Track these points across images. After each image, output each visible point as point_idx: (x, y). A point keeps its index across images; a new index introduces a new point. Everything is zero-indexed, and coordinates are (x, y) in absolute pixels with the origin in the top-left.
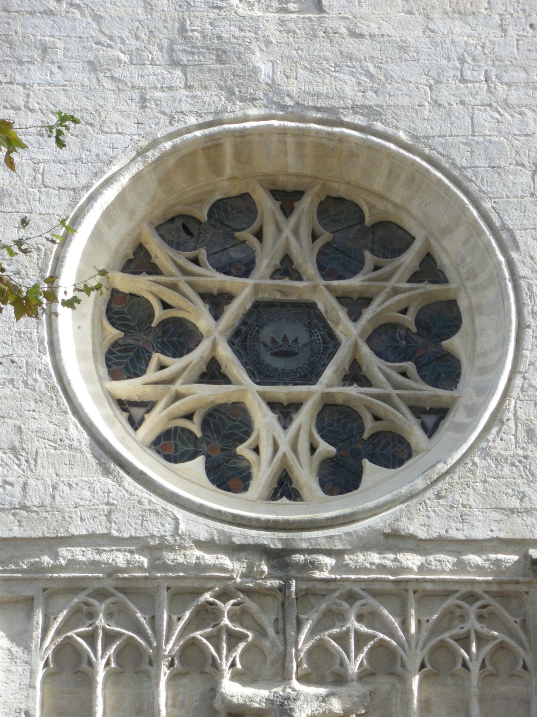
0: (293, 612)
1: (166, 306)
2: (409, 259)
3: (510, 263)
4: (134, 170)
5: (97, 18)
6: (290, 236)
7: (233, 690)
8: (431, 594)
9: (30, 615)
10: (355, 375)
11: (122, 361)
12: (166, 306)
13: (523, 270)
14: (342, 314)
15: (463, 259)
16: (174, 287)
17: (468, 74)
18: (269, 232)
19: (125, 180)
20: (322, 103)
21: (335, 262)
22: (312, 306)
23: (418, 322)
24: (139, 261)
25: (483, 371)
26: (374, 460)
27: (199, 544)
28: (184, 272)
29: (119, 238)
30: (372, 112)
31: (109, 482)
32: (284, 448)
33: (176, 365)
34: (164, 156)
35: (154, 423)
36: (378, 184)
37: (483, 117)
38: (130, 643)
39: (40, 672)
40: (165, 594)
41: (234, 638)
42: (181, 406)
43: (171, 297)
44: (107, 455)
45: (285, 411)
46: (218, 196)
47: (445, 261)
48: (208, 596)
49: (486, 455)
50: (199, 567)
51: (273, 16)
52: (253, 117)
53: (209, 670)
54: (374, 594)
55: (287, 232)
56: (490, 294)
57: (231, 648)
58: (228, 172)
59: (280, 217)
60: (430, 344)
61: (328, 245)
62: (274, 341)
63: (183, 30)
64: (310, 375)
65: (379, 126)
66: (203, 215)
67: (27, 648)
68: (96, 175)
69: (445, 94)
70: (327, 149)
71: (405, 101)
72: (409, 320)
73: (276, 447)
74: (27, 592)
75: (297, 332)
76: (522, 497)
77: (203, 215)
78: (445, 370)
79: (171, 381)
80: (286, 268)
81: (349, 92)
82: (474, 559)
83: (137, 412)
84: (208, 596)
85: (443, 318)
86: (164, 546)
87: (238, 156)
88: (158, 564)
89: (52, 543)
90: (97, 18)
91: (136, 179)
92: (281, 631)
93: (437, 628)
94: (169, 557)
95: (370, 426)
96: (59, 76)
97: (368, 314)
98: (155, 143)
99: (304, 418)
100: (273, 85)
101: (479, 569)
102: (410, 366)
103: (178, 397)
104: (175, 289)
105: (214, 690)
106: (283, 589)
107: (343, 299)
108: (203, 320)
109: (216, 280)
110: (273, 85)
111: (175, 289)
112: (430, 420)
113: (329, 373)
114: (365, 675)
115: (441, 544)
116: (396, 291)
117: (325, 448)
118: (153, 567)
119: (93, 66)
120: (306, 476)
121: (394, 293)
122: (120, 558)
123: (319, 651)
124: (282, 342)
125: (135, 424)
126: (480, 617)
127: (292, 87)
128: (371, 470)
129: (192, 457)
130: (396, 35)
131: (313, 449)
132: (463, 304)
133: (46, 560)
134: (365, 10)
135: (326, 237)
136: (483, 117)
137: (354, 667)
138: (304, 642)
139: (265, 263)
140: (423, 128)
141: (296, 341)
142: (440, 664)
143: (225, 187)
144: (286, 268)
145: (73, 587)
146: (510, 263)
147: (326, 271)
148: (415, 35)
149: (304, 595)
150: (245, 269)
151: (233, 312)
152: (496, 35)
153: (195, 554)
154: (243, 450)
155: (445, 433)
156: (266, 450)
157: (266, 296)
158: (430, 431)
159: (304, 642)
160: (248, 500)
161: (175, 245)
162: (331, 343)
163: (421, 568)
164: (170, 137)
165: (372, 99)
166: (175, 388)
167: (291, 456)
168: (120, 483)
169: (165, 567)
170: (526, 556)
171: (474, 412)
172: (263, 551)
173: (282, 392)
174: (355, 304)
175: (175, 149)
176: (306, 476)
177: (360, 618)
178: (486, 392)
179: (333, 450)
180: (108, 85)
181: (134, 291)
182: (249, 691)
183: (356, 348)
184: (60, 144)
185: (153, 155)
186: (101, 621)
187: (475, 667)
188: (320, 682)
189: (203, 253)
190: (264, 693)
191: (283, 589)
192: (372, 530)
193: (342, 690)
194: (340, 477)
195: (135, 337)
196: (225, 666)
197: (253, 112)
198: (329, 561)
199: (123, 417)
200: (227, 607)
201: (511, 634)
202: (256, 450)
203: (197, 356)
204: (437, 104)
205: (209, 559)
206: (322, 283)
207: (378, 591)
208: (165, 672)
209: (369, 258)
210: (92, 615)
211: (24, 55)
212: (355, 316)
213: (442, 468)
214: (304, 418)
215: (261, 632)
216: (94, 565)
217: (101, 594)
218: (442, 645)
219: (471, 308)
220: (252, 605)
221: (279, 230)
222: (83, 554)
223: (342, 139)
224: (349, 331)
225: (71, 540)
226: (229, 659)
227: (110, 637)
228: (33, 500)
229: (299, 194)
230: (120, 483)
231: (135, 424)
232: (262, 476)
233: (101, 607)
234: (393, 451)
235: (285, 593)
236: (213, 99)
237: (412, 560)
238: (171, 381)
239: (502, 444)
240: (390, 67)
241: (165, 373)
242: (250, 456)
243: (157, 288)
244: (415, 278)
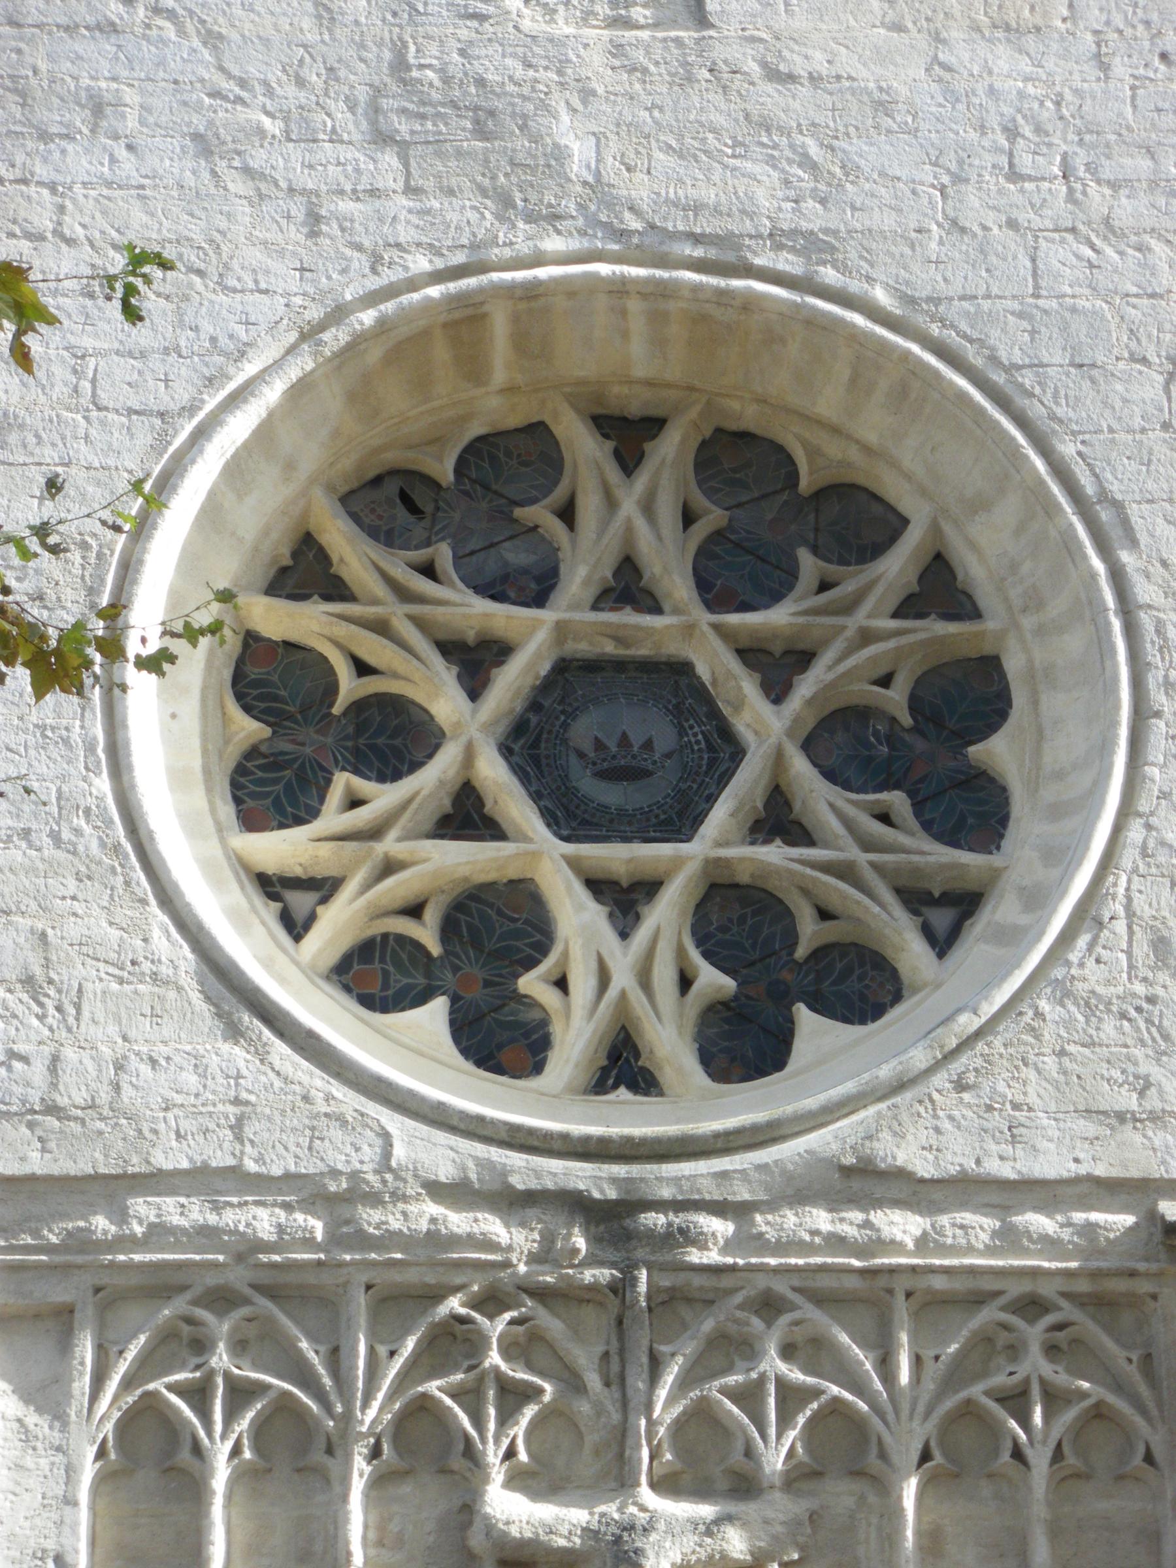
0: (641, 1338)
1: (363, 669)
2: (897, 567)
3: (1117, 576)
4: (294, 372)
5: (213, 39)
6: (635, 516)
7: (509, 1509)
8: (943, 1298)
9: (65, 1344)
10: (777, 819)
11: (267, 789)
12: (363, 669)
13: (1144, 591)
14: (749, 687)
15: (1014, 567)
16: (381, 628)
17: (1025, 162)
18: (589, 507)
19: (273, 393)
20: (705, 225)
21: (734, 573)
22: (684, 669)
23: (915, 703)
24: (303, 571)
25: (1057, 811)
26: (820, 1006)
27: (436, 1190)
28: (404, 594)
29: (260, 520)
30: (814, 245)
31: (238, 1054)
32: (623, 979)
33: (385, 797)
34: (358, 341)
35: (337, 924)
36: (828, 403)
37: (1059, 256)
38: (284, 1406)
39: (88, 1471)
40: (361, 1300)
41: (513, 1396)
42: (396, 888)
43: (373, 649)
44: (234, 995)
45: (624, 899)
46: (477, 429)
47: (975, 571)
48: (455, 1304)
49: (1064, 994)
50: (436, 1239)
52: (553, 255)
53: (457, 1465)
54: (820, 1299)
55: (629, 507)
56: (1074, 643)
57: (506, 1418)
58: (500, 376)
59: (613, 474)
60: (941, 752)
61: (717, 536)
63: (400, 65)
64: (679, 821)
65: (829, 275)
66: (445, 470)
67: (59, 1417)
68: (211, 382)
69: (974, 206)
70: (716, 326)
71: (888, 221)
72: (896, 699)
73: (604, 979)
74: (60, 1294)
75: (650, 727)
76: (1144, 1086)
77: (445, 470)
78: (974, 810)
79: (374, 833)
80: (627, 587)
81: (764, 202)
82: (1039, 1222)
83: (300, 901)
84: (455, 1304)
85: (970, 696)
86: (358, 1193)
87: (521, 342)
88: (345, 1234)
89: (113, 1188)
90: (213, 39)
91: (299, 391)
92: (616, 1380)
93: (958, 1374)
94: (371, 1218)
95: (810, 932)
96: (128, 165)
97: (806, 687)
98: (339, 314)
99: (665, 915)
100: (597, 185)
101: (1050, 1245)
102: (897, 800)
103: (389, 868)
104: (382, 632)
105: (468, 1509)
106: (620, 1288)
107: (751, 653)
108: (444, 699)
109: (474, 612)
110: (597, 185)
111: (382, 632)
112: (941, 919)
113: (721, 815)
114: (800, 1477)
115: (966, 1189)
116: (866, 637)
117: (713, 980)
118: (335, 1240)
119: (204, 145)
120: (670, 1042)
121: (863, 641)
122: (263, 1221)
123: (700, 1423)
124: (619, 748)
125: (296, 927)
126: (1052, 1350)
127: (640, 189)
128: (812, 1029)
129: (421, 998)
130: (867, 77)
131: (685, 982)
132: (1013, 665)
133: (101, 1224)
134: (800, 22)
135: (713, 517)
136: (1059, 256)
138: (665, 1404)
139: (580, 575)
140: (925, 280)
141: (648, 745)
142: (964, 1451)
143: (492, 409)
144: (627, 587)
145: (160, 1284)
146: (1117, 576)
147: (714, 592)
148: (908, 77)
149: (666, 1302)
150: (538, 588)
151: (510, 682)
152: (1086, 76)
153: (427, 1212)
154: (532, 983)
155: (974, 947)
156: (582, 983)
157: (582, 648)
158: (942, 943)
159: (665, 1404)
161: (384, 535)
162: (725, 749)
163: (923, 1243)
164: (372, 299)
165: (814, 217)
166: (382, 848)
167: (637, 998)
168: (262, 1056)
169: (362, 1241)
170: (1153, 1217)
171: (1039, 900)
172: (576, 1204)
173: (618, 856)
174: (778, 665)
175: (383, 326)
176: (670, 1042)
177: (788, 1352)
178: (1063, 858)
179: (728, 984)
180: (237, 185)
181: (294, 636)
182: (546, 1511)
183: (779, 760)
184: (132, 314)
185: (335, 338)
186: (221, 1359)
187: (1039, 1459)
188: (700, 1492)
189: (444, 554)
190: (579, 1516)
191: (620, 1288)
192: (814, 1160)
193: (750, 1509)
194: (745, 1044)
195: (297, 736)
196: (493, 1455)
197: (554, 244)
198: (720, 1227)
199: (269, 912)
200: (497, 1327)
201: (1119, 1386)
202: (562, 984)
203: (431, 779)
204: (956, 227)
205: (458, 1221)
206: (705, 618)
207: (828, 1293)
208: (360, 1469)
209: (808, 563)
210: (201, 1346)
211: (53, 119)
212: (777, 692)
213: (968, 1023)
214: (665, 915)
215: (572, 1382)
216: (206, 1235)
217: (222, 1300)
218: (969, 1411)
220: (551, 1324)
221: (611, 503)
222: (181, 1211)
223: (750, 303)
224: (765, 724)
225: (156, 1182)
226: (501, 1442)
227: (240, 1394)
228: (73, 1094)
229: (654, 425)
230: (262, 1056)
231: (296, 927)
232: (575, 1040)
233: (222, 1328)
234: (861, 987)
235: (624, 1297)
236: (467, 217)
237: (902, 1226)
238: (374, 833)
239: (1100, 970)
240: (854, 146)
241: (361, 816)
242: (548, 997)
243: (343, 630)
244: (910, 607)
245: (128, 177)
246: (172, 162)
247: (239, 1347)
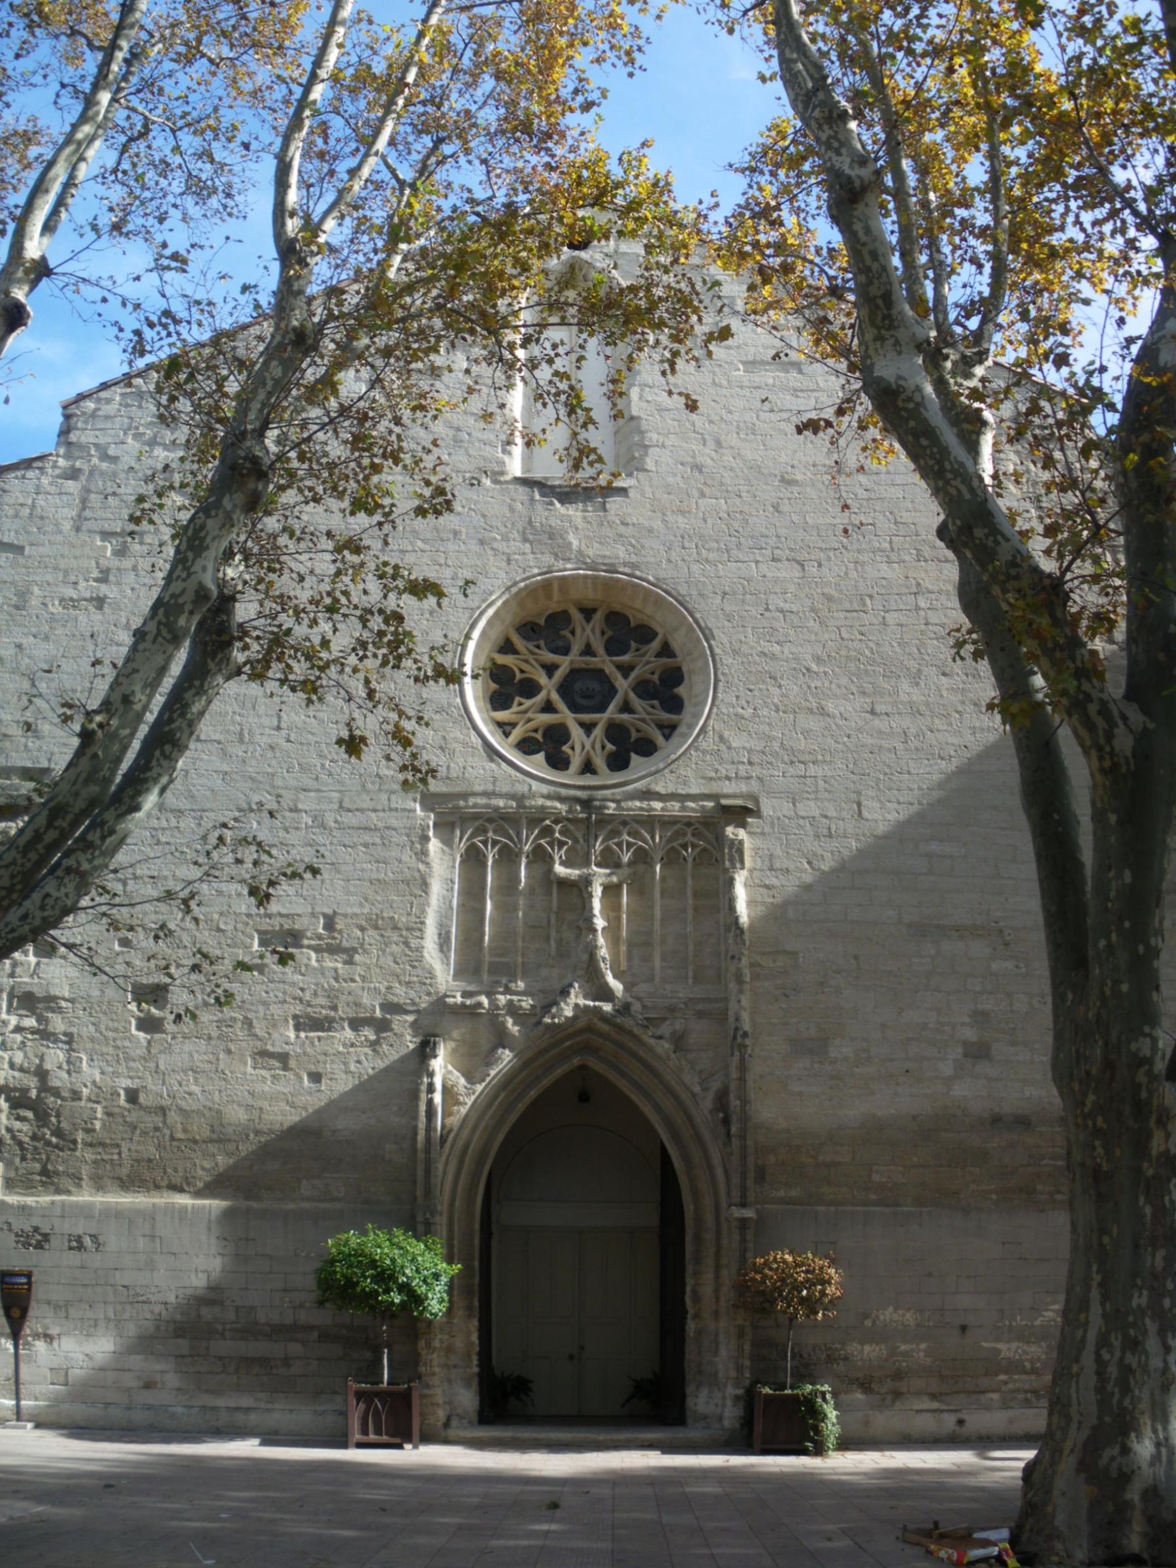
0: (593, 831)
1: (522, 671)
2: (655, 645)
3: (710, 647)
4: (504, 598)
5: (484, 516)
6: (589, 633)
7: (560, 870)
8: (666, 822)
9: (453, 831)
10: (626, 708)
11: (498, 701)
12: (522, 671)
13: (717, 651)
14: (619, 676)
16: (526, 661)
17: (686, 544)
18: (578, 630)
19: (499, 603)
20: (607, 561)
21: (615, 647)
22: (602, 671)
23: (660, 679)
24: (507, 647)
25: (696, 705)
26: (637, 753)
27: (543, 797)
28: (532, 653)
29: (496, 634)
30: (634, 566)
31: (493, 765)
32: (588, 747)
33: (528, 703)
34: (520, 590)
35: (517, 734)
36: (638, 604)
37: (695, 568)
38: (506, 845)
39: (458, 860)
40: (524, 822)
41: (561, 844)
42: (531, 725)
43: (525, 666)
44: (492, 753)
45: (588, 728)
47: (675, 646)
48: (548, 822)
49: (697, 749)
50: (543, 807)
51: (579, 514)
52: (569, 569)
53: (549, 860)
54: (637, 822)
55: (588, 631)
56: (699, 664)
57: (560, 849)
60: (668, 691)
61: (610, 638)
63: (530, 522)
64: (602, 708)
65: (638, 573)
66: (542, 622)
67: (451, 847)
68: (484, 601)
69: (674, 556)
70: (610, 586)
71: (652, 560)
72: (655, 678)
73: (583, 747)
74: (451, 818)
75: (594, 686)
76: (717, 771)
77: (542, 622)
78: (675, 705)
79: (525, 712)
80: (588, 651)
81: (621, 555)
82: (691, 804)
83: (508, 728)
84: (548, 822)
85: (674, 677)
86: (523, 797)
87: (561, 589)
88: (521, 805)
89: (465, 796)
90: (484, 516)
91: (504, 603)
92: (587, 840)
93: (670, 840)
94: (527, 803)
95: (634, 735)
96: (463, 547)
97: (633, 675)
98: (515, 584)
99: (598, 732)
100: (580, 552)
101: (693, 810)
102: (656, 703)
103: (529, 720)
104: (525, 662)
105: (550, 869)
106: (588, 819)
107: (620, 667)
108: (543, 679)
109: (550, 657)
110: (580, 552)
111: (525, 662)
112: (667, 731)
113: (612, 707)
114: (631, 863)
115: (673, 796)
116: (648, 663)
117: (610, 747)
118: (518, 807)
119: (482, 542)
120: (599, 762)
121: (647, 663)
122: (501, 803)
123: (607, 851)
124: (584, 691)
125: (507, 735)
126: (694, 835)
127: (590, 552)
128: (635, 759)
129: (537, 752)
130: (646, 524)
131: (603, 747)
132: (685, 669)
133: (462, 803)
134: (630, 510)
135: (609, 633)
136: (695, 568)
137: (626, 858)
138: (598, 846)
139: (577, 647)
140: (662, 574)
142: (671, 858)
143: (554, 607)
144: (588, 651)
145: (476, 817)
146: (710, 647)
147: (610, 652)
148: (657, 524)
149: (598, 822)
150: (566, 651)
151: (559, 675)
152: (700, 523)
153: (540, 802)
154: (565, 748)
155: (675, 739)
156: (578, 748)
157: (577, 666)
158: (667, 737)
159: (598, 846)
161: (526, 638)
162: (613, 691)
163: (663, 809)
164: (524, 580)
165: (634, 559)
166: (528, 715)
168: (499, 765)
169: (525, 807)
170: (718, 804)
171: (691, 727)
172: (578, 800)
173: (587, 717)
174: (626, 670)
175: (526, 587)
176: (599, 762)
177: (629, 834)
178: (697, 716)
180: (490, 552)
182: (569, 871)
183: (626, 693)
184: (466, 595)
185: (514, 590)
186: (490, 834)
187: (690, 860)
188: (606, 867)
189: (542, 643)
190: (577, 872)
191: (588, 819)
192: (635, 790)
193: (619, 871)
194: (618, 762)
195: (505, 688)
196: (556, 858)
197: (569, 566)
198: (613, 805)
199: (500, 731)
200: (558, 828)
201: (709, 843)
202: (573, 748)
203: (540, 698)
204: (669, 561)
205: (549, 803)
206: (608, 658)
207: (638, 820)
208: (524, 861)
209: (633, 645)
210: (485, 831)
211: (444, 536)
212: (626, 676)
213: (673, 757)
214: (598, 732)
215: (576, 841)
216: (487, 806)
217: (490, 820)
218: (673, 848)
220: (571, 827)
221: (584, 630)
222: (481, 801)
223: (618, 580)
224: (622, 684)
225: (474, 794)
226: (558, 855)
227: (495, 843)
228: (453, 774)
229: (594, 610)
230: (499, 765)
231: (507, 735)
232: (576, 762)
233: (490, 827)
234: (647, 748)
235: (588, 823)
236: (548, 559)
237: (657, 805)
238: (525, 712)
239: (708, 743)
240: (643, 541)
241: (522, 708)
242: (569, 751)
244: (659, 655)
245: (484, 338)
246: (474, 546)
247: (495, 832)
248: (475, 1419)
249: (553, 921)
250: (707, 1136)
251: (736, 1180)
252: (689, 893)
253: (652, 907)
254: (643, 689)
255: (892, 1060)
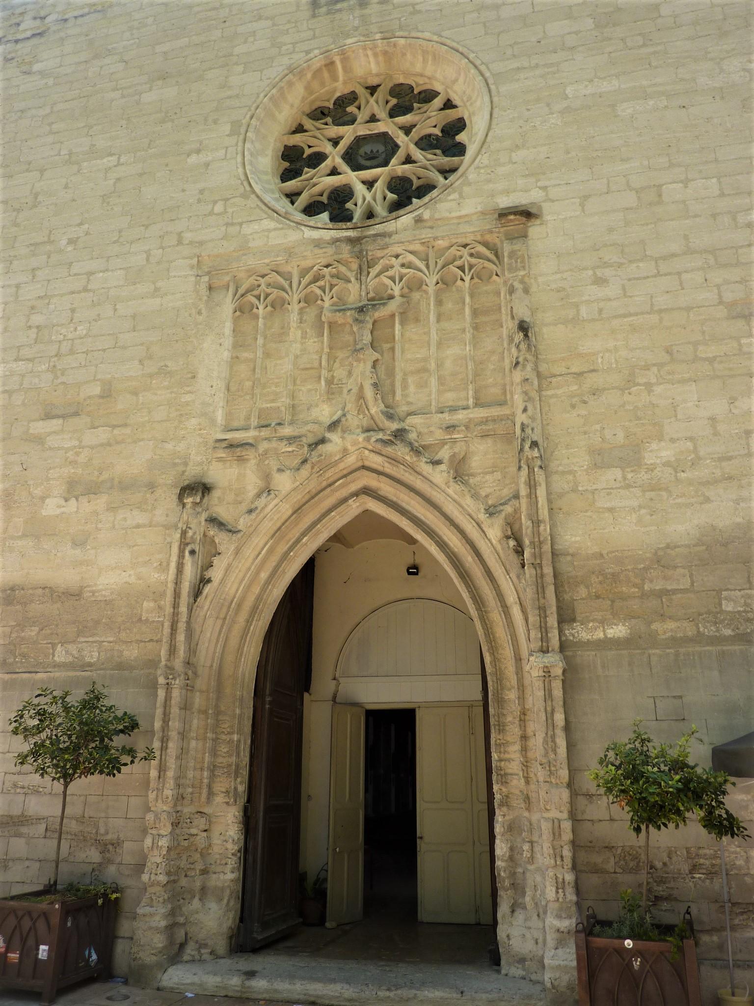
10: (409, 160)
15: (464, 92)
46: (338, 94)
47: (456, 100)
58: (341, 78)
59: (368, 96)
62: (366, 153)
73: (364, 199)
102: (438, 152)
113: (393, 161)
141: (378, 151)
160: (483, 531)
167: (372, 202)
173: (368, 174)
179: (395, 196)
181: (295, 144)
202: (356, 205)
219: (470, 116)
221: (368, 102)
224: (385, 126)
232: (358, 214)
243: (304, 138)
248: (221, 946)
249: (324, 363)
250: (498, 572)
251: (533, 619)
252: (467, 311)
253: (428, 333)
254: (426, 143)
255: (730, 458)
